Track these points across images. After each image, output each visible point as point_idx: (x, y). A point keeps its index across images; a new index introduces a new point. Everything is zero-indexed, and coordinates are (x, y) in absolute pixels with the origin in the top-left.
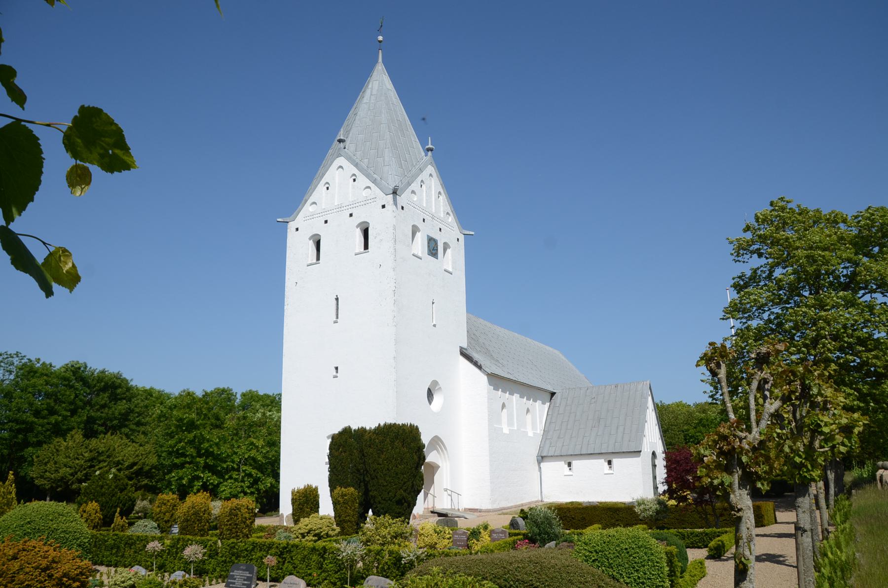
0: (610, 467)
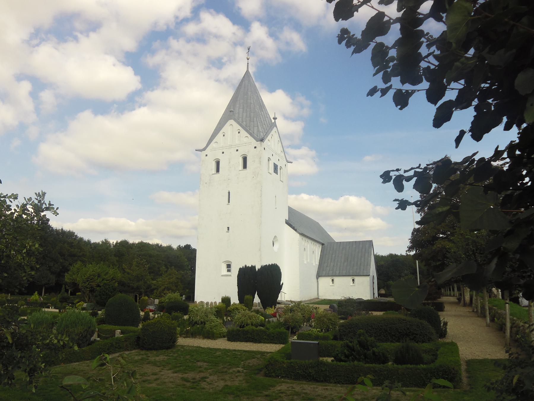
0: (353, 283)
